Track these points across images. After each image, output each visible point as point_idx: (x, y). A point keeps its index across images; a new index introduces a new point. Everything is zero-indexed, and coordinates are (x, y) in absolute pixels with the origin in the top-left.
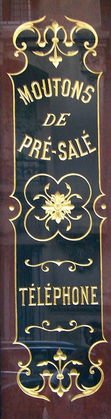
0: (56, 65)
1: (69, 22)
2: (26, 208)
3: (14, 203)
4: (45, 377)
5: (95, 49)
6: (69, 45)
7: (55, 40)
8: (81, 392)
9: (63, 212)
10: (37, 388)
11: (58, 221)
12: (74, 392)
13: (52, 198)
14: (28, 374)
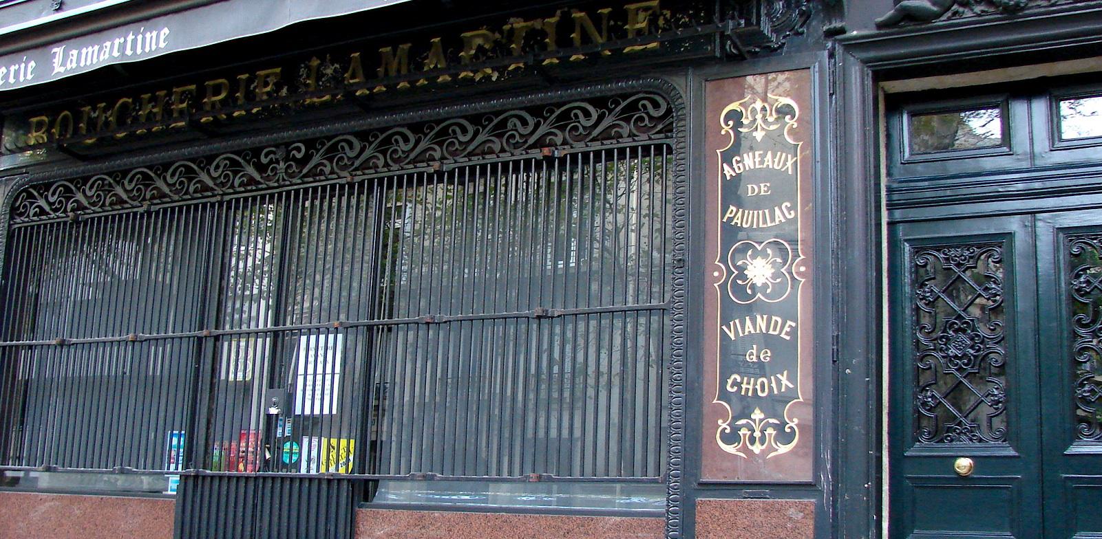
3: (799, 273)
14: (728, 431)
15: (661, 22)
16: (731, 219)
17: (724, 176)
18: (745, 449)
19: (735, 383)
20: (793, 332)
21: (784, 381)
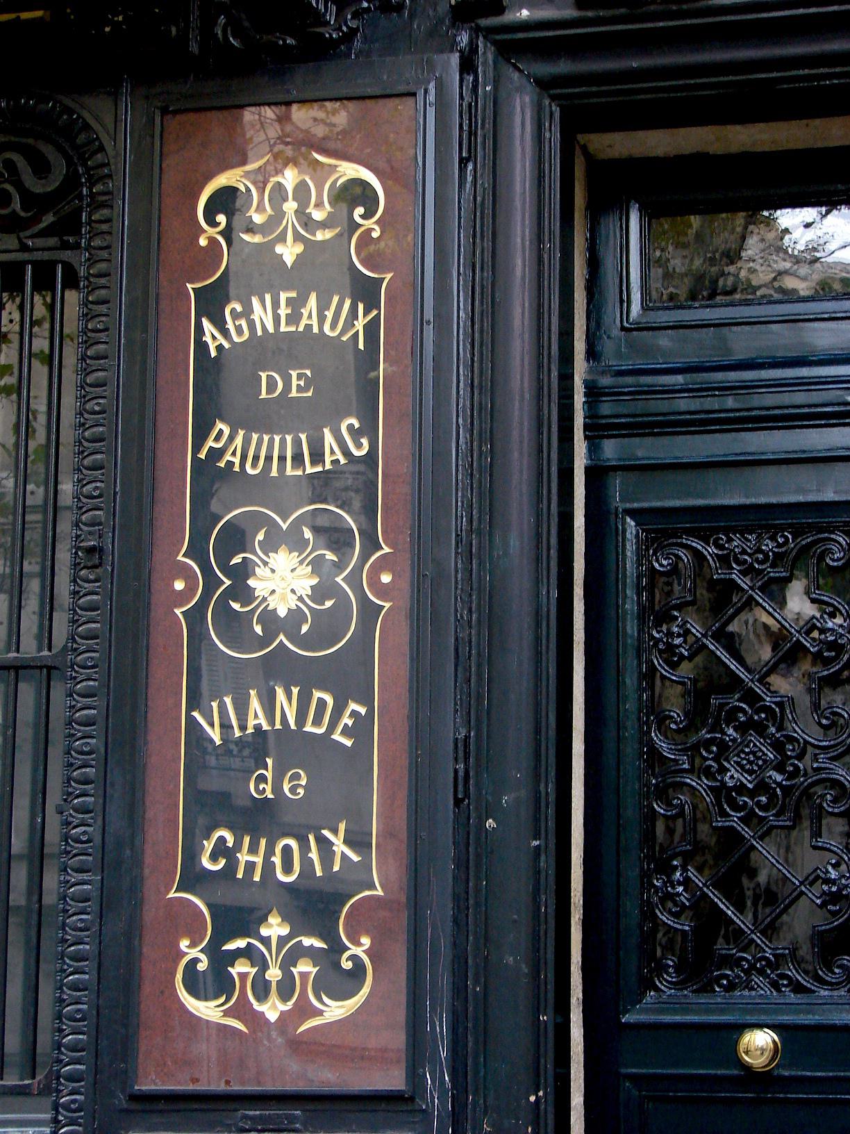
0: (289, 260)
1: (322, 164)
2: (211, 582)
3: (382, 591)
4: (239, 974)
5: (376, 223)
8: (321, 1013)
9: (293, 591)
10: (223, 999)
11: (282, 613)
13: (270, 561)
14: (202, 966)
16: (216, 454)
17: (202, 347)
18: (242, 1010)
19: (220, 850)
20: (361, 729)
21: (340, 847)
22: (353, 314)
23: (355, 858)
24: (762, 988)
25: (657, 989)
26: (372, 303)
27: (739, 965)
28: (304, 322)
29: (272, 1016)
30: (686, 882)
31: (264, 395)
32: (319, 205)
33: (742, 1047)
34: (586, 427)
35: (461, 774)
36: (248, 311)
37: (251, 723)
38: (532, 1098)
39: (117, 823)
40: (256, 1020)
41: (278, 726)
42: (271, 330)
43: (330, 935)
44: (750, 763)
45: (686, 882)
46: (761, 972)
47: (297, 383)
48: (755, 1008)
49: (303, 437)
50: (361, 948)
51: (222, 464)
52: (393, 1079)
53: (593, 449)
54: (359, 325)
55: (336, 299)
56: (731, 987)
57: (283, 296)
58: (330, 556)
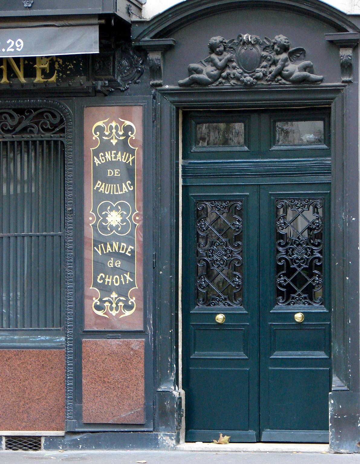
0: (114, 144)
2: (98, 218)
6: (121, 133)
7: (114, 131)
8: (124, 314)
10: (103, 311)
11: (114, 226)
12: (121, 313)
15: (57, 66)
16: (98, 189)
17: (94, 164)
21: (128, 278)
22: (129, 157)
23: (132, 280)
24: (221, 306)
25: (198, 305)
26: (133, 155)
27: (216, 300)
28: (118, 158)
29: (114, 315)
30: (205, 281)
31: (109, 175)
32: (121, 131)
33: (216, 318)
34: (182, 176)
35: (154, 262)
36: (105, 155)
37: (108, 250)
38: (170, 331)
39: (78, 273)
40: (118, 121)
41: (114, 251)
42: (110, 160)
43: (126, 297)
44: (219, 254)
45: (205, 281)
46: (221, 301)
47: (116, 172)
48: (220, 310)
49: (118, 185)
50: (133, 300)
51: (100, 191)
52: (140, 328)
53: (184, 181)
54: (130, 160)
55: (125, 153)
56: (214, 305)
57: (113, 152)
58: (125, 213)
